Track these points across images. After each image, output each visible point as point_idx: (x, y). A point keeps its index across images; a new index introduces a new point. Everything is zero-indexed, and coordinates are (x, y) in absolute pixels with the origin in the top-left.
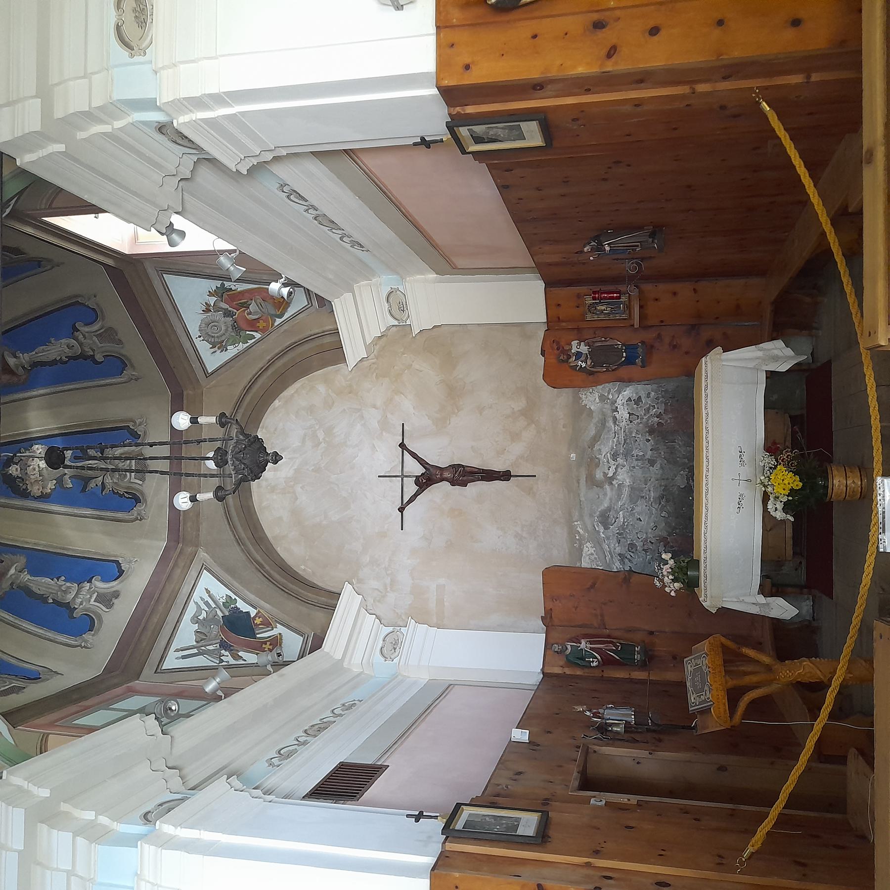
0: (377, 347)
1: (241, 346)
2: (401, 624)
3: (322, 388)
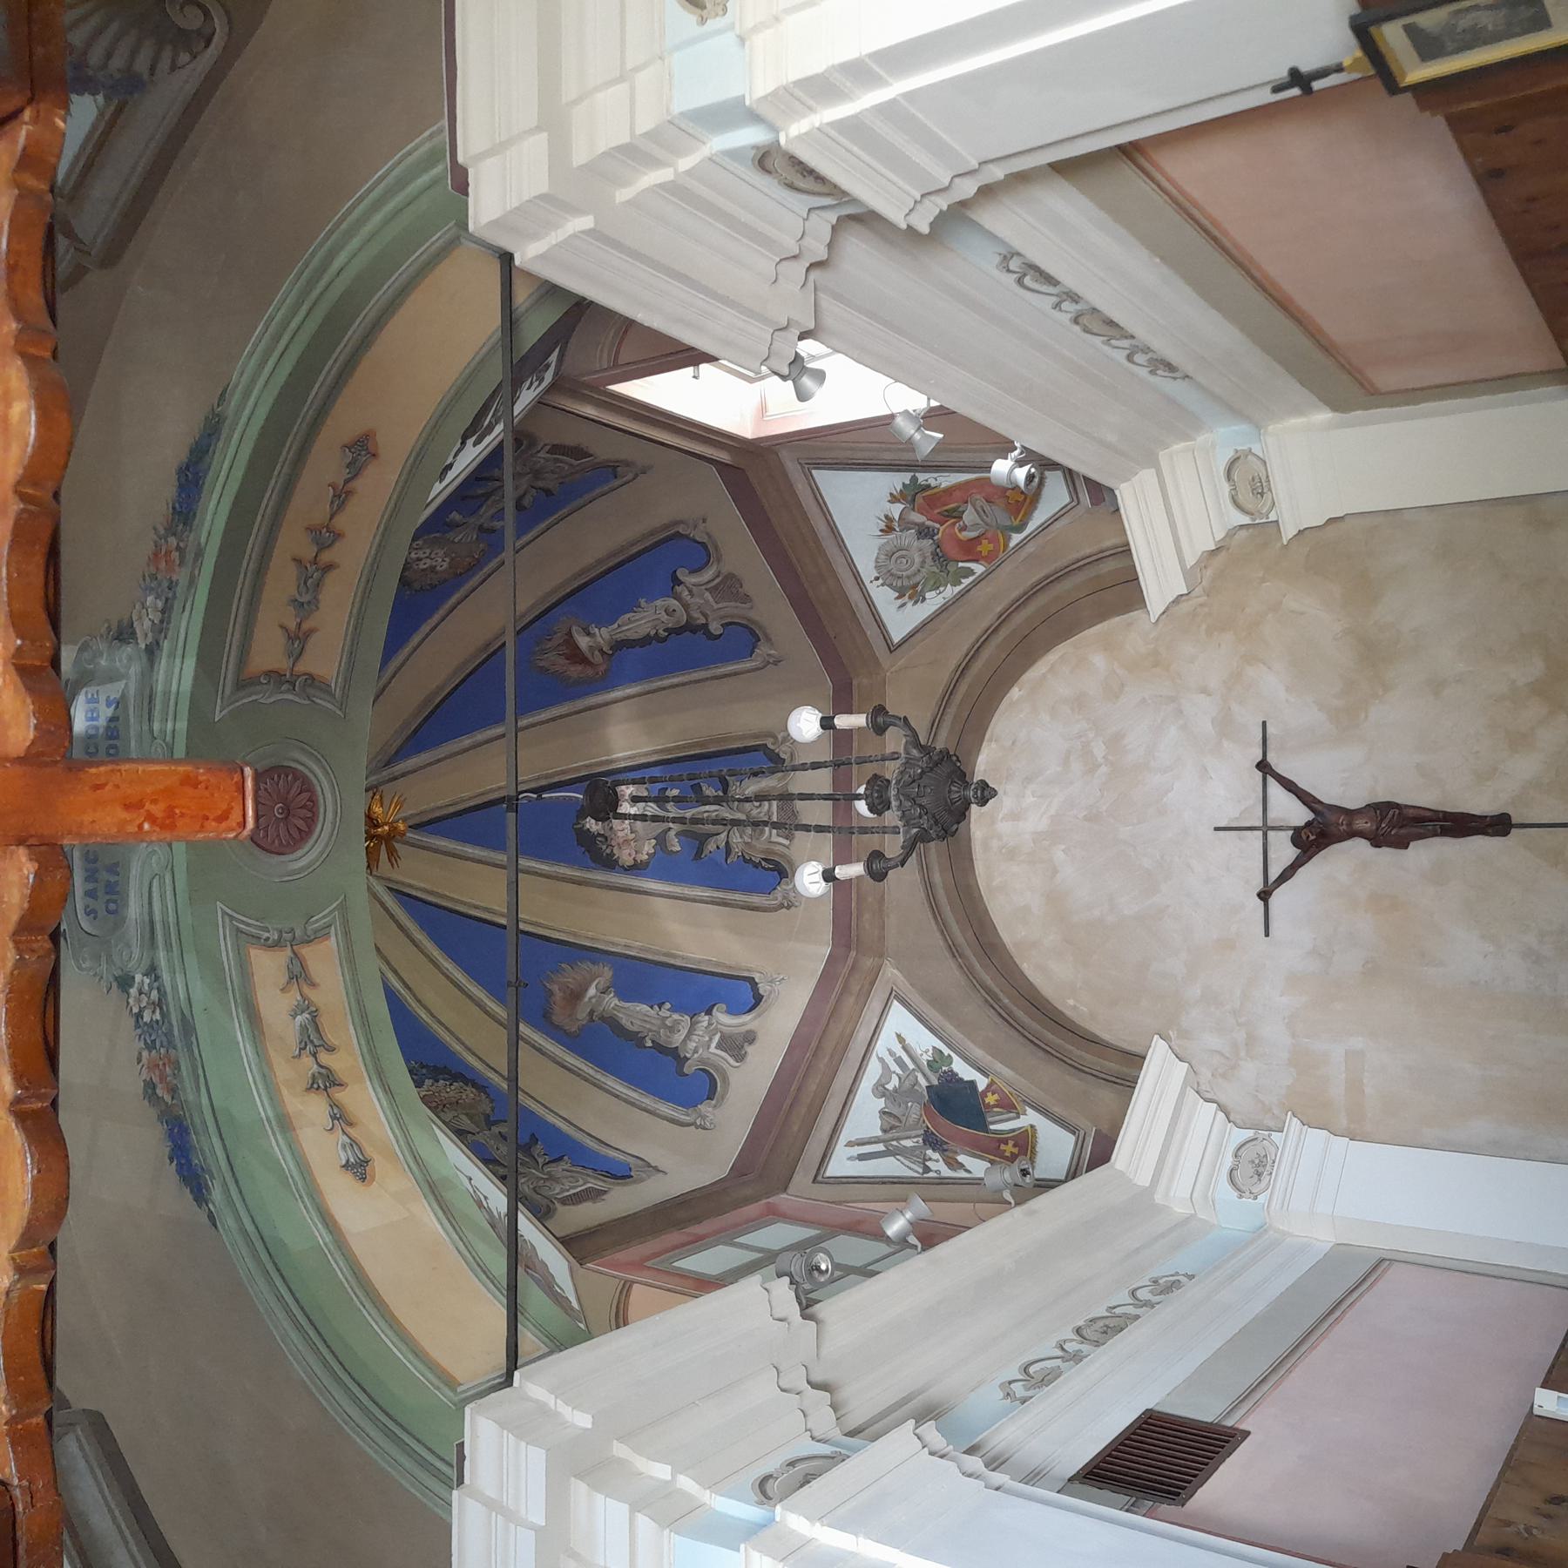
0: (1209, 573)
1: (950, 591)
2: (1271, 1124)
3: (1099, 660)
